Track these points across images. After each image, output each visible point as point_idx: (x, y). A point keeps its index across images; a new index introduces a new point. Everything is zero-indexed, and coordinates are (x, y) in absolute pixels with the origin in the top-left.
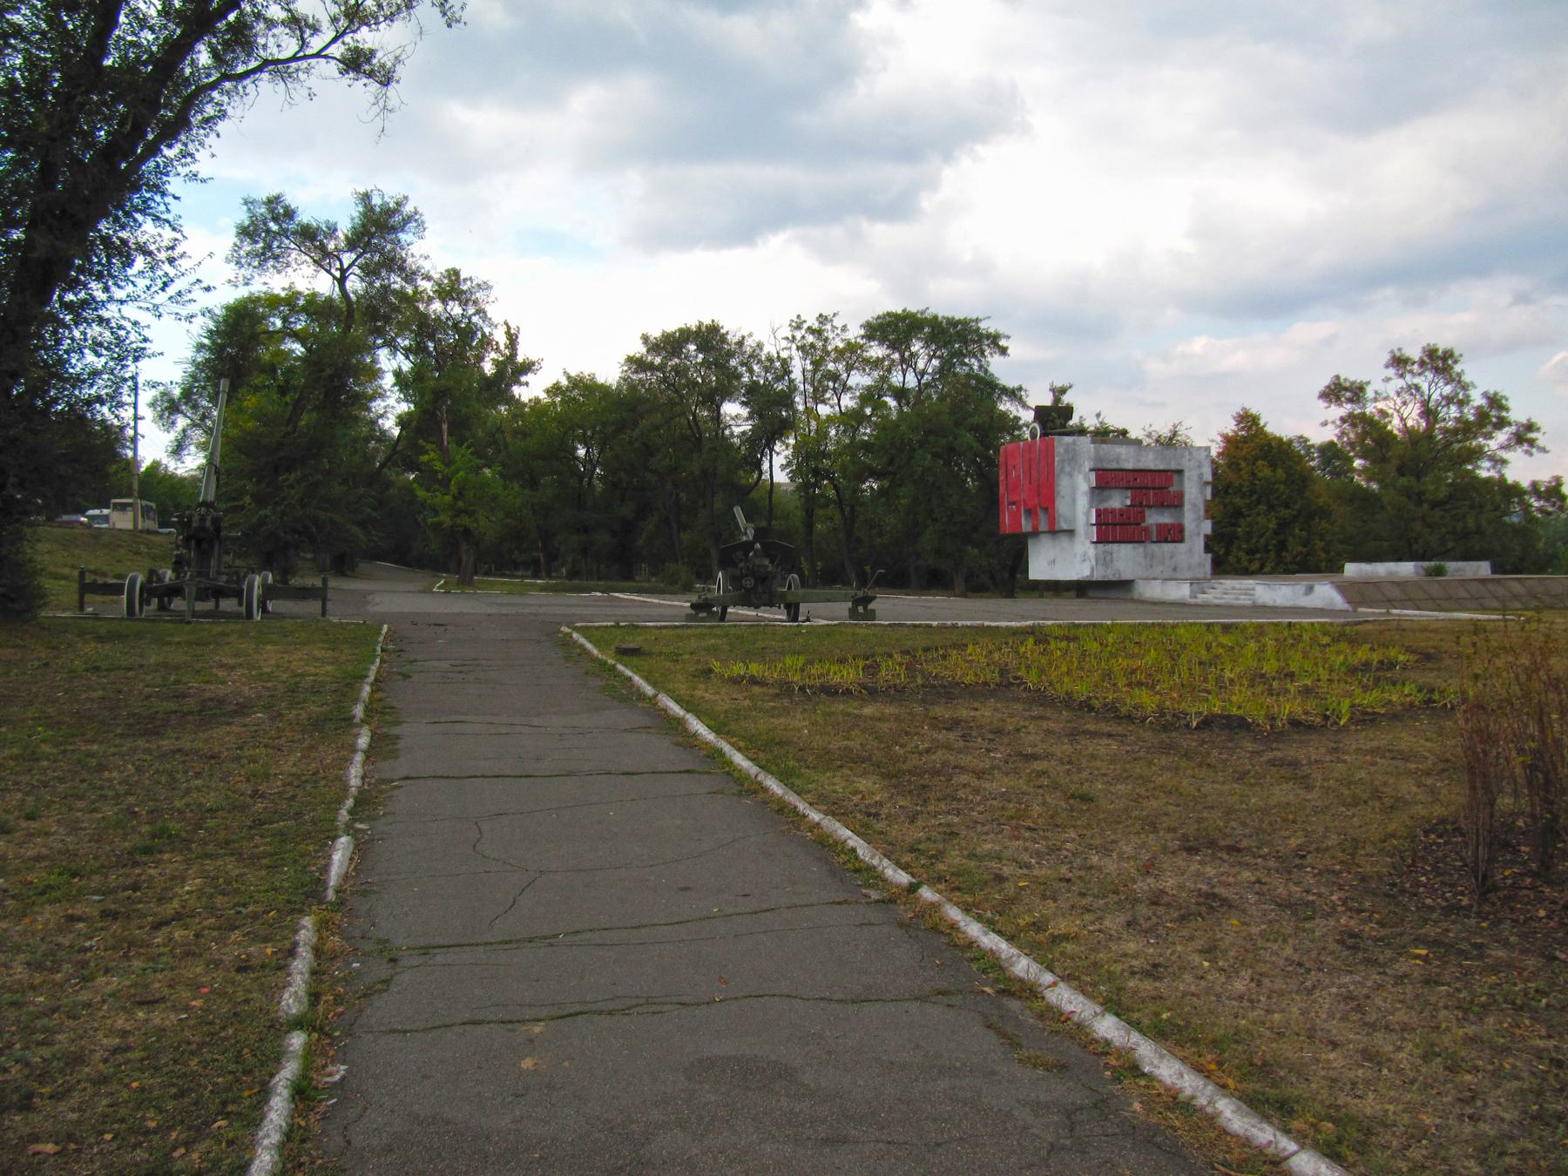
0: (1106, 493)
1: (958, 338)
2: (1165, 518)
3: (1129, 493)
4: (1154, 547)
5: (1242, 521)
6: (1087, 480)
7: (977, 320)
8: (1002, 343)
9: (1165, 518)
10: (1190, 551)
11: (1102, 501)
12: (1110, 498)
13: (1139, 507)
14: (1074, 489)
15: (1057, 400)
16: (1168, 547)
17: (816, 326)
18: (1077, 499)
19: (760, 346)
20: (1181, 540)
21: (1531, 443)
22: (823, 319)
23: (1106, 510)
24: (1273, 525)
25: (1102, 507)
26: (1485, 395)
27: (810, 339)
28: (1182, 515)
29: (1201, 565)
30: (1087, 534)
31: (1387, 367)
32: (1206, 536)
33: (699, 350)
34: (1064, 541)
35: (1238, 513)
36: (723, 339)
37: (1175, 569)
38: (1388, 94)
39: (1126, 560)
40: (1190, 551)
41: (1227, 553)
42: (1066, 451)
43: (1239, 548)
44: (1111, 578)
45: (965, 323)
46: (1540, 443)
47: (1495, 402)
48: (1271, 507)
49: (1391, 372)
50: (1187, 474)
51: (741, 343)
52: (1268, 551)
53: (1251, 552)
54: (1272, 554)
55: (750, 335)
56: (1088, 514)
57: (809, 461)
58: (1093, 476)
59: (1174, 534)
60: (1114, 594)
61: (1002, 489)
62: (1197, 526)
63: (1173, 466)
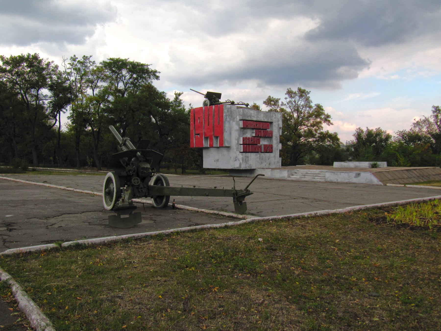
0: (245, 131)
1: (140, 71)
3: (254, 131)
4: (262, 154)
6: (238, 124)
7: (147, 65)
8: (157, 74)
10: (275, 156)
11: (244, 134)
12: (247, 133)
13: (258, 138)
14: (231, 129)
15: (177, 98)
16: (267, 155)
17: (82, 60)
18: (233, 133)
19: (57, 67)
20: (272, 152)
21: (329, 121)
22: (85, 58)
23: (246, 138)
25: (245, 136)
26: (315, 105)
27: (79, 66)
29: (278, 162)
30: (237, 148)
31: (286, 94)
32: (280, 150)
33: (28, 66)
34: (224, 151)
36: (40, 61)
37: (270, 164)
38: (225, 24)
39: (253, 160)
40: (275, 156)
42: (228, 111)
44: (248, 168)
45: (142, 65)
46: (331, 122)
47: (319, 108)
49: (287, 96)
50: (274, 124)
51: (48, 64)
55: (53, 62)
56: (238, 140)
57: (80, 119)
58: (241, 123)
59: (269, 149)
60: (243, 175)
61: (192, 128)
62: (277, 146)
63: (270, 121)
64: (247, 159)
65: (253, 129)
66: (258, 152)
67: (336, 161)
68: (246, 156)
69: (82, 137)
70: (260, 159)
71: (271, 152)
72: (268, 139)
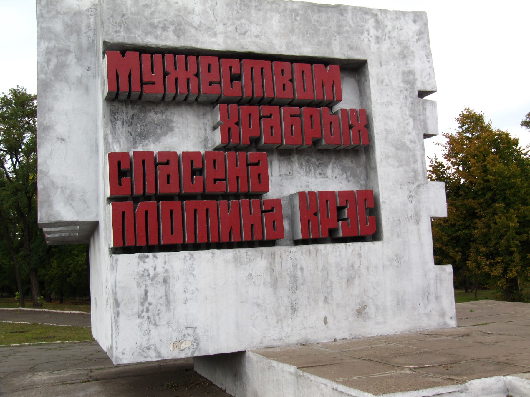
2: (333, 180)
5: (479, 223)
9: (333, 180)
10: (398, 260)
12: (167, 128)
13: (247, 150)
20: (374, 235)
23: (144, 158)
24: (513, 224)
28: (370, 168)
32: (437, 224)
35: (472, 215)
37: (361, 312)
40: (398, 260)
41: (465, 258)
43: (477, 252)
48: (509, 205)
50: (372, 70)
52: (511, 253)
53: (490, 256)
54: (517, 257)
59: (351, 220)
63: (338, 51)
64: (156, 294)
65: (213, 104)
66: (272, 243)
67: (454, 269)
68: (144, 275)
69: (458, 257)
70: (275, 284)
71: (372, 233)
72: (348, 162)
